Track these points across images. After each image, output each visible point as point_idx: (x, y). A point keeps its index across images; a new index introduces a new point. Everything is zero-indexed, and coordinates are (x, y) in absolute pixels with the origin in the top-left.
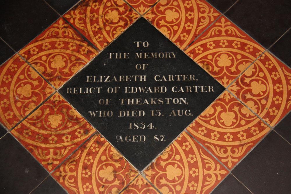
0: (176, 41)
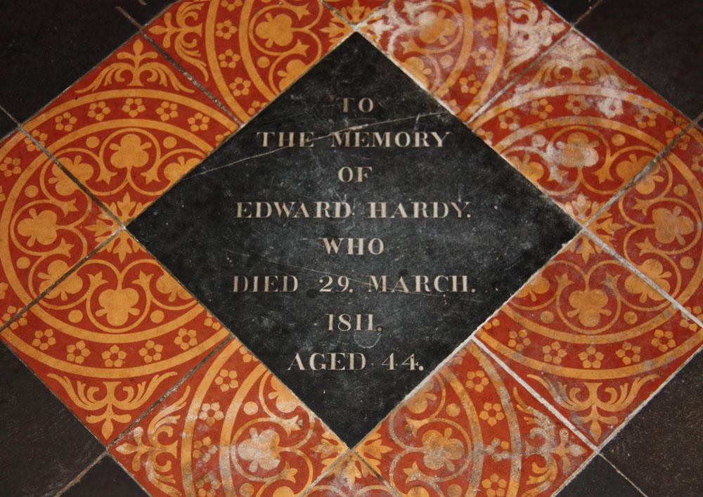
0: (252, 366)
